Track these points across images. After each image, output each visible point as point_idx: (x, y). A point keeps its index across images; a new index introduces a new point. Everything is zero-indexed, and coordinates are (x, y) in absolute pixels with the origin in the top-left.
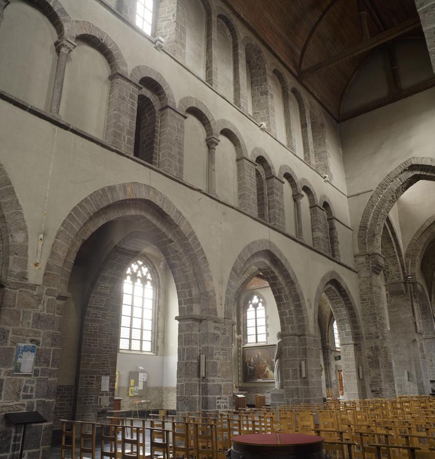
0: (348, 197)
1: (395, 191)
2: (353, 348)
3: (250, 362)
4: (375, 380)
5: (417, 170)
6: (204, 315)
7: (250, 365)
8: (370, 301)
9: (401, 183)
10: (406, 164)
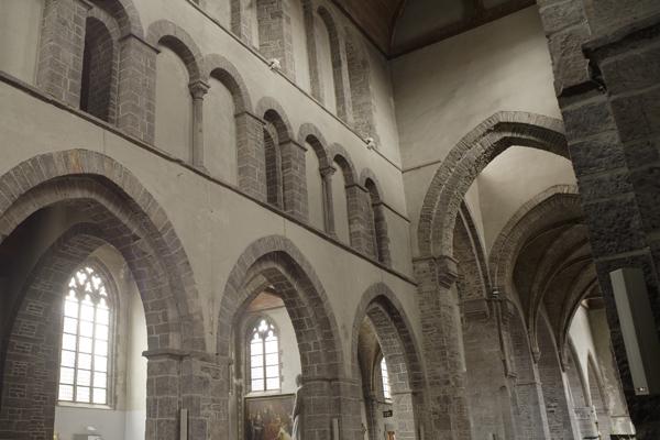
2: (410, 399)
3: (255, 420)
6: (187, 349)
7: (255, 424)
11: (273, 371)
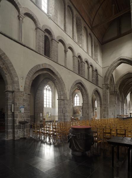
11: (78, 102)
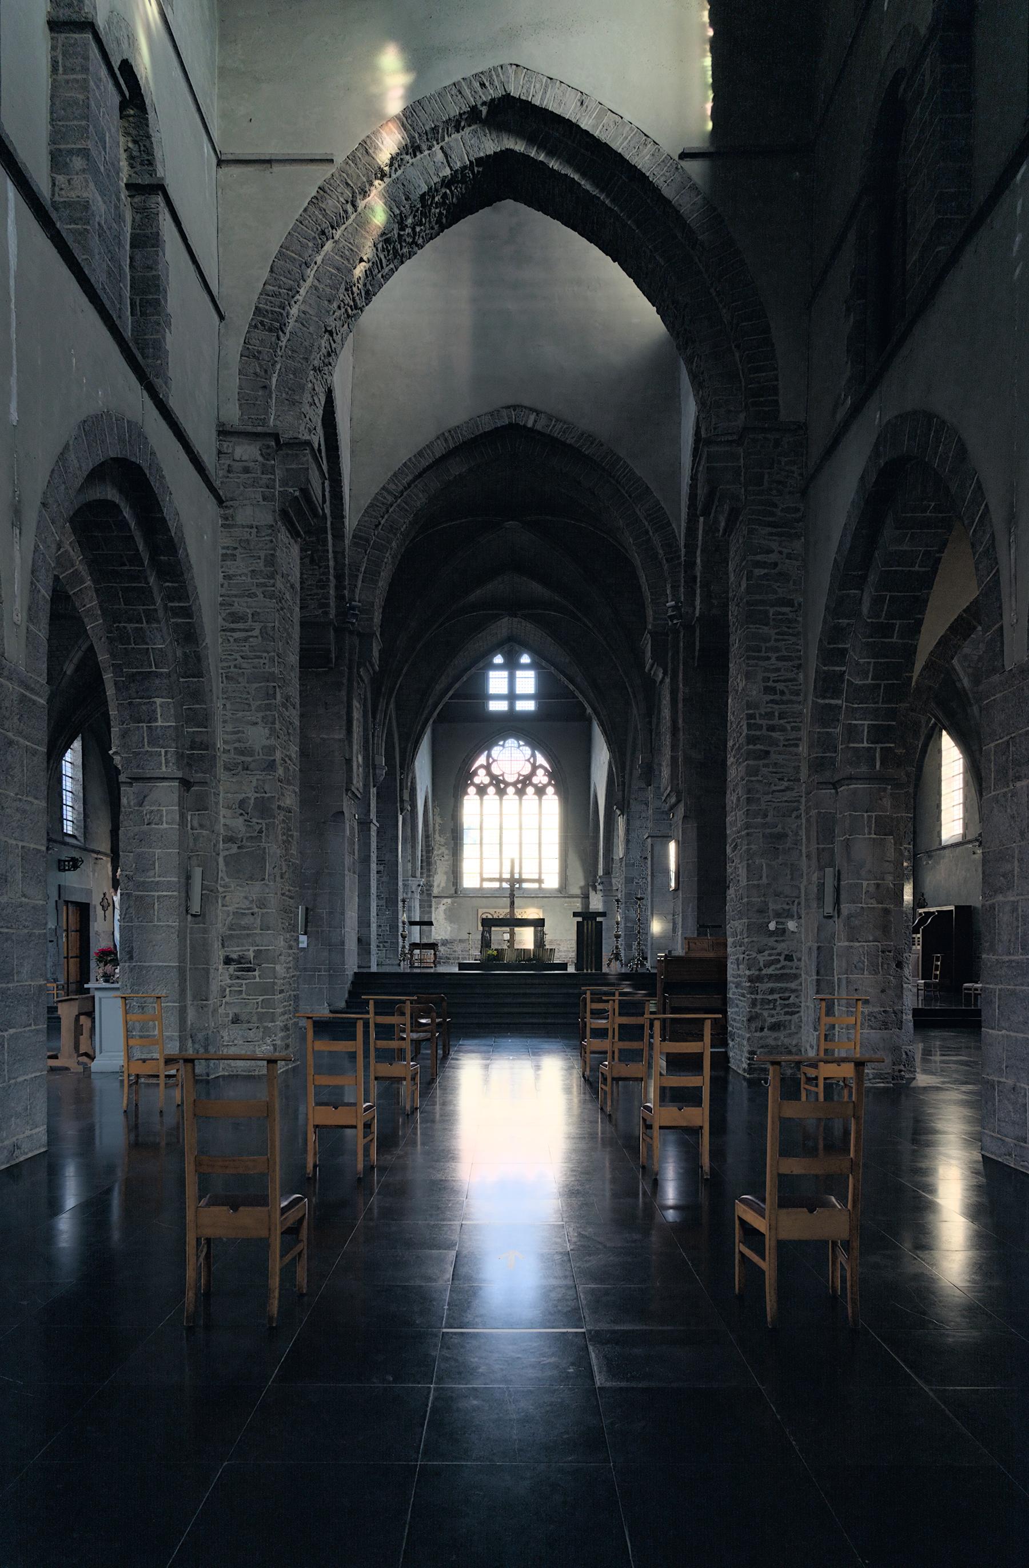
0: (220, 163)
1: (415, 196)
4: (246, 921)
5: (518, 133)
8: (258, 626)
9: (447, 172)
10: (483, 85)
